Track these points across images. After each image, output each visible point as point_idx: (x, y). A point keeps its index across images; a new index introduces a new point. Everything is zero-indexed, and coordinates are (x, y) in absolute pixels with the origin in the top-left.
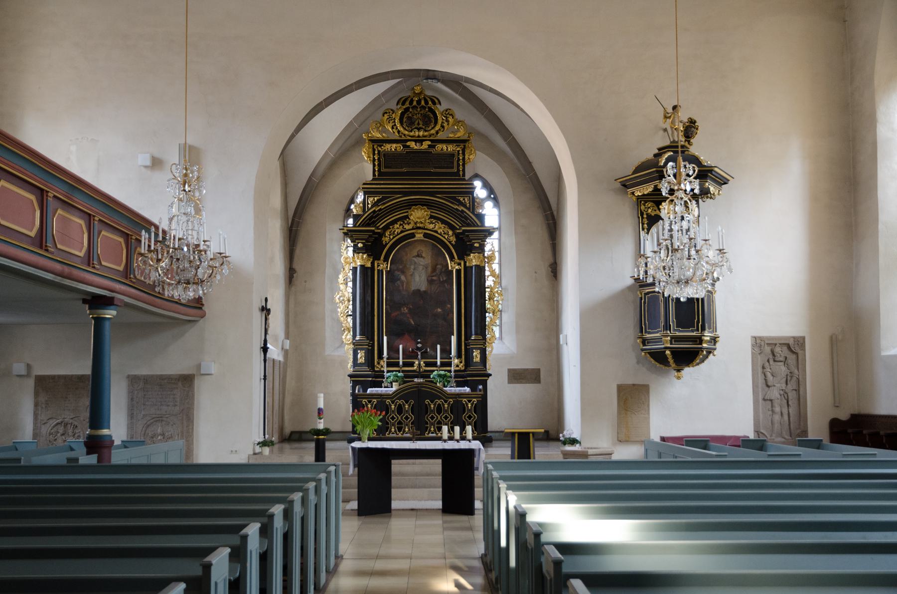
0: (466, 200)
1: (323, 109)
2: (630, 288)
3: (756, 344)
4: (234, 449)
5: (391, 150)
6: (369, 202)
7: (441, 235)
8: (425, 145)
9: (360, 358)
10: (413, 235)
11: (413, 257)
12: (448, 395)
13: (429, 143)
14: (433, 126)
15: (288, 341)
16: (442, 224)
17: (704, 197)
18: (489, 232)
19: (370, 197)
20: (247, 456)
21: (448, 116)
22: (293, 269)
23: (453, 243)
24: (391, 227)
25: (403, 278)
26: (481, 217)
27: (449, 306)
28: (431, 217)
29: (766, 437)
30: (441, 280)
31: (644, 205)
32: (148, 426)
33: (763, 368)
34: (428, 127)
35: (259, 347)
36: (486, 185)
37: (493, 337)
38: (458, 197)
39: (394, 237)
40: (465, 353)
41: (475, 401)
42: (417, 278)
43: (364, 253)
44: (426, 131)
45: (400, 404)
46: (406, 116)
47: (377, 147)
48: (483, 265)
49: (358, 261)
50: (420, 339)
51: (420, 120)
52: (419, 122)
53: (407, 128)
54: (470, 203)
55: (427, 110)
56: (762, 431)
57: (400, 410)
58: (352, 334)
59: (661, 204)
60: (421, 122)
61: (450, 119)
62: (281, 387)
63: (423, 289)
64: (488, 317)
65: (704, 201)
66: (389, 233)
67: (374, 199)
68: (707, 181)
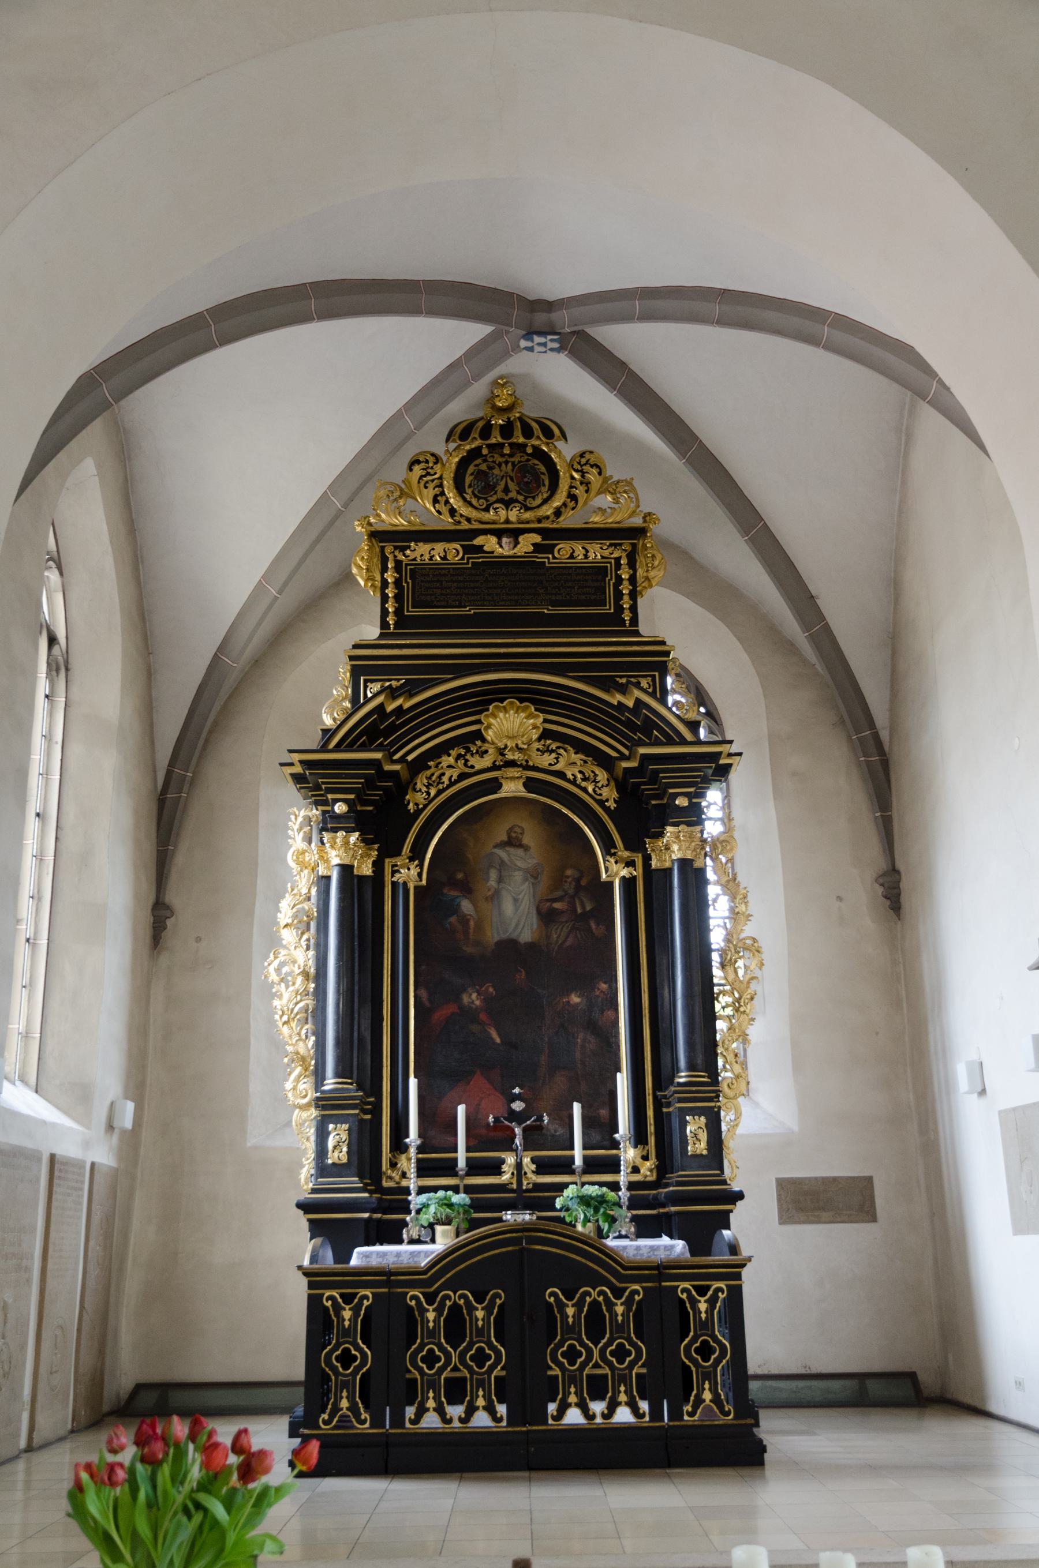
7: (574, 782)
8: (526, 543)
9: (335, 1147)
11: (495, 847)
13: (537, 538)
14: (545, 496)
19: (372, 681)
21: (586, 468)
23: (612, 805)
24: (431, 763)
25: (466, 906)
27: (604, 986)
28: (545, 735)
30: (579, 911)
34: (534, 498)
39: (439, 792)
42: (508, 907)
43: (349, 831)
44: (527, 509)
45: (455, 1307)
46: (471, 469)
50: (521, 1088)
53: (474, 501)
60: (512, 486)
61: (592, 476)
66: (425, 781)
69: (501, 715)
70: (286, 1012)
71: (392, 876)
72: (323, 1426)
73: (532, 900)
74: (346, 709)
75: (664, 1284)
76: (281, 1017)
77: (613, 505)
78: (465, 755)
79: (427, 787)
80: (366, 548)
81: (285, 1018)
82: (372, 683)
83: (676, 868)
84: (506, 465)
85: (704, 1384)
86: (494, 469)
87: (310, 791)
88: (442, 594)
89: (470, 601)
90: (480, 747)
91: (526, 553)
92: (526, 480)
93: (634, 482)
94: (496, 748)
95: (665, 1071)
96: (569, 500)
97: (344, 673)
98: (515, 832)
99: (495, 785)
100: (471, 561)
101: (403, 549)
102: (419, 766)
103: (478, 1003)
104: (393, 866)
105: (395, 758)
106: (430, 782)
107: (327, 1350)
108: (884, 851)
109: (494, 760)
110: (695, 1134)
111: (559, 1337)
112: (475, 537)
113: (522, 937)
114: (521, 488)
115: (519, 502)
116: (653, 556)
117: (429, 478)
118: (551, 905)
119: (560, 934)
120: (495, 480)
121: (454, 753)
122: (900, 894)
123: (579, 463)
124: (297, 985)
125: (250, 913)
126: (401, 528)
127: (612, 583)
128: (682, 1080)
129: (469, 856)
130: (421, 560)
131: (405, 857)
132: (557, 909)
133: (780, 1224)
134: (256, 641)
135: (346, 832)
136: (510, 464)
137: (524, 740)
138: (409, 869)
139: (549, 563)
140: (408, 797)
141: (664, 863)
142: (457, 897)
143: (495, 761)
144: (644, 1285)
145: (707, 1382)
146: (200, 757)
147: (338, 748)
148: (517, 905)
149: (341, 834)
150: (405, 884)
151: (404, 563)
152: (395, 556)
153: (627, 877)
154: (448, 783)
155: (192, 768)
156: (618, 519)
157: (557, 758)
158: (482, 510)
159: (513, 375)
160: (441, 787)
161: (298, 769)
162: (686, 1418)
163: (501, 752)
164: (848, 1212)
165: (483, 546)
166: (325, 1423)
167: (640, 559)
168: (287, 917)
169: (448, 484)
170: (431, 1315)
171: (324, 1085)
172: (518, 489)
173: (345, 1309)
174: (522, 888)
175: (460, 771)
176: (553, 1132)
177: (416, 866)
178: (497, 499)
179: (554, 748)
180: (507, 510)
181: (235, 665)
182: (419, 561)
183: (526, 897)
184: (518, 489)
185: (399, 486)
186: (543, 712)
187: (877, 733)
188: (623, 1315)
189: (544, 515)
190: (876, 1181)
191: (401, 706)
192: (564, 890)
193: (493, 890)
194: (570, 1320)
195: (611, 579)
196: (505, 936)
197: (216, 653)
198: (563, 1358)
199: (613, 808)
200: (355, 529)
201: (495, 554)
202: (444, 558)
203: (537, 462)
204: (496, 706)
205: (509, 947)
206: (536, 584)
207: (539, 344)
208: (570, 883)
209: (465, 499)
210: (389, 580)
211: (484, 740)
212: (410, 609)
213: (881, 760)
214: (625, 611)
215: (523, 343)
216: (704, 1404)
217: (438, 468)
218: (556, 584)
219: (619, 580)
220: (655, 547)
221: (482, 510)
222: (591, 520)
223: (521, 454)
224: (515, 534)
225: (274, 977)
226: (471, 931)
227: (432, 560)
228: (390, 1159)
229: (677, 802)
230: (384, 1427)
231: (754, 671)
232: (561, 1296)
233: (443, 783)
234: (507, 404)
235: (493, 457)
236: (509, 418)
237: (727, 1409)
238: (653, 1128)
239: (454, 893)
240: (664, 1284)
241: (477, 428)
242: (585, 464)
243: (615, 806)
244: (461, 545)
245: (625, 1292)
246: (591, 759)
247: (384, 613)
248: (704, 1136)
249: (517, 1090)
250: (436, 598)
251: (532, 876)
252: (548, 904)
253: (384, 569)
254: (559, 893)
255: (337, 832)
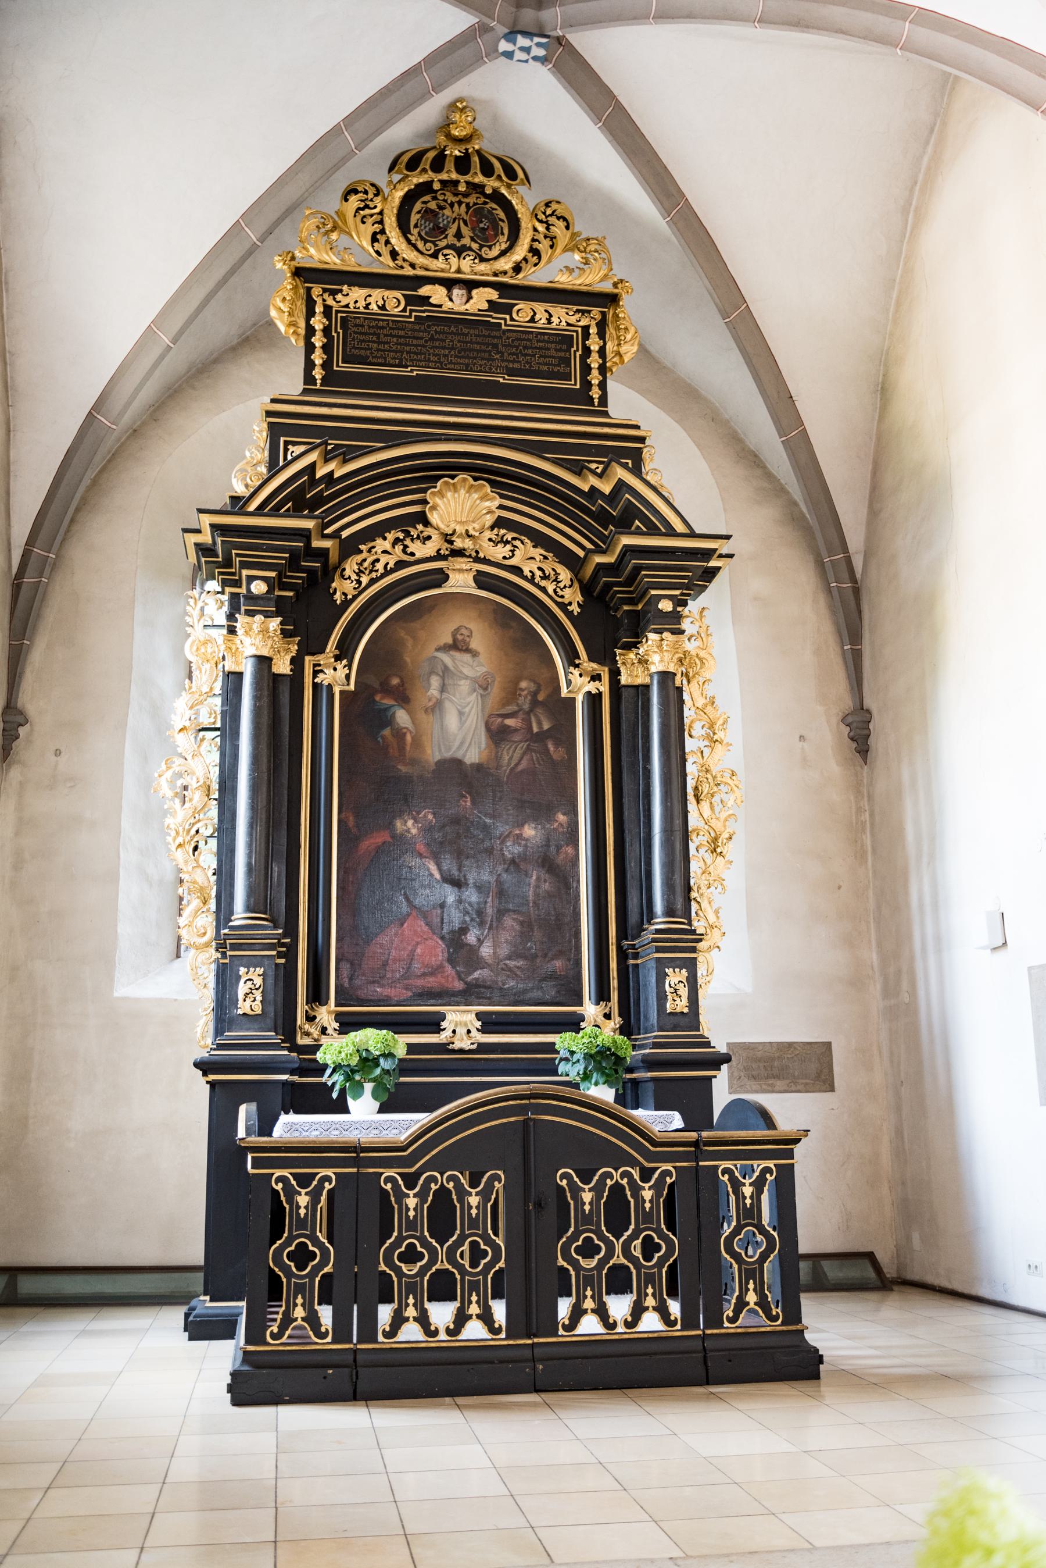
7: (531, 580)
8: (481, 298)
11: (438, 649)
13: (493, 295)
14: (504, 246)
19: (295, 444)
21: (552, 220)
23: (575, 609)
24: (362, 547)
25: (402, 717)
28: (500, 523)
30: (535, 729)
34: (490, 247)
39: (373, 581)
42: (452, 721)
44: (483, 260)
45: (443, 1191)
46: (418, 206)
53: (420, 245)
61: (559, 228)
66: (356, 567)
69: (449, 494)
70: (181, 833)
71: (315, 676)
72: (271, 1341)
73: (480, 715)
74: (261, 474)
75: (701, 1163)
76: (174, 840)
77: (582, 266)
78: (404, 539)
79: (358, 574)
80: (289, 287)
81: (180, 840)
82: (294, 445)
83: (655, 682)
85: (747, 1283)
86: (445, 209)
87: (217, 568)
88: (378, 350)
89: (412, 360)
90: (422, 532)
91: (479, 310)
92: (482, 225)
93: (606, 242)
94: (442, 533)
95: (633, 918)
96: (531, 254)
97: (260, 432)
98: (462, 634)
99: (440, 578)
100: (414, 314)
101: (333, 293)
102: (349, 547)
103: (414, 831)
104: (315, 665)
105: (327, 532)
106: (361, 568)
107: (277, 1245)
108: (852, 689)
109: (438, 548)
110: (676, 989)
111: (572, 1229)
112: (420, 287)
113: (467, 757)
114: (476, 235)
115: (474, 251)
116: (626, 329)
117: (367, 212)
118: (502, 722)
119: (512, 755)
120: (445, 222)
121: (391, 536)
122: (869, 736)
123: (544, 213)
124: (195, 802)
125: (122, 725)
126: (332, 267)
127: (578, 354)
129: (408, 660)
130: (355, 308)
131: (332, 655)
132: (509, 727)
134: (137, 405)
135: (265, 617)
136: (464, 205)
137: (477, 526)
138: (335, 669)
139: (506, 325)
140: (334, 585)
141: (635, 678)
142: (393, 706)
143: (440, 550)
144: (678, 1164)
145: (751, 1282)
146: (64, 540)
147: (260, 511)
148: (463, 719)
149: (259, 618)
150: (330, 687)
151: (334, 309)
152: (324, 300)
153: (593, 692)
154: (383, 571)
155: (55, 549)
156: (587, 282)
157: (513, 551)
158: (428, 255)
159: (474, 100)
160: (374, 575)
161: (206, 538)
162: (726, 1324)
163: (448, 538)
164: (804, 1081)
165: (429, 297)
166: (274, 1336)
167: (610, 331)
168: (184, 719)
169: (391, 222)
170: (412, 1202)
171: (231, 921)
172: (472, 235)
173: (300, 1194)
174: (468, 700)
176: (500, 984)
177: (345, 667)
179: (509, 539)
181: (114, 427)
182: (352, 309)
183: (474, 711)
184: (472, 235)
185: (332, 218)
186: (502, 496)
188: (651, 1201)
189: (501, 269)
190: (835, 1047)
191: (332, 472)
192: (518, 705)
193: (434, 700)
194: (587, 1208)
195: (578, 350)
196: (448, 755)
198: (577, 1254)
199: (576, 614)
200: (274, 265)
201: (444, 308)
202: (383, 308)
203: (495, 206)
204: (431, 493)
205: (453, 767)
206: (490, 348)
207: (522, 49)
208: (526, 697)
209: (409, 241)
210: (317, 327)
211: (427, 523)
212: (340, 364)
213: (853, 587)
214: (593, 387)
215: (504, 46)
216: (747, 1308)
217: (378, 200)
218: (514, 350)
219: (587, 351)
220: (627, 319)
221: (428, 255)
222: (556, 280)
223: (478, 195)
224: (470, 285)
225: (166, 791)
226: (408, 748)
227: (368, 309)
228: (307, 1011)
229: (660, 606)
230: (351, 1341)
231: (714, 481)
232: (576, 1179)
233: (377, 571)
234: (465, 133)
235: (445, 195)
236: (467, 150)
237: (774, 1313)
238: (616, 981)
239: (388, 702)
240: (701, 1163)
241: (427, 159)
242: (550, 215)
243: (579, 610)
244: (403, 295)
245: (654, 1173)
246: (551, 555)
247: (309, 365)
248: (684, 991)
250: (371, 353)
251: (480, 686)
252: (499, 720)
253: (310, 313)
254: (513, 708)
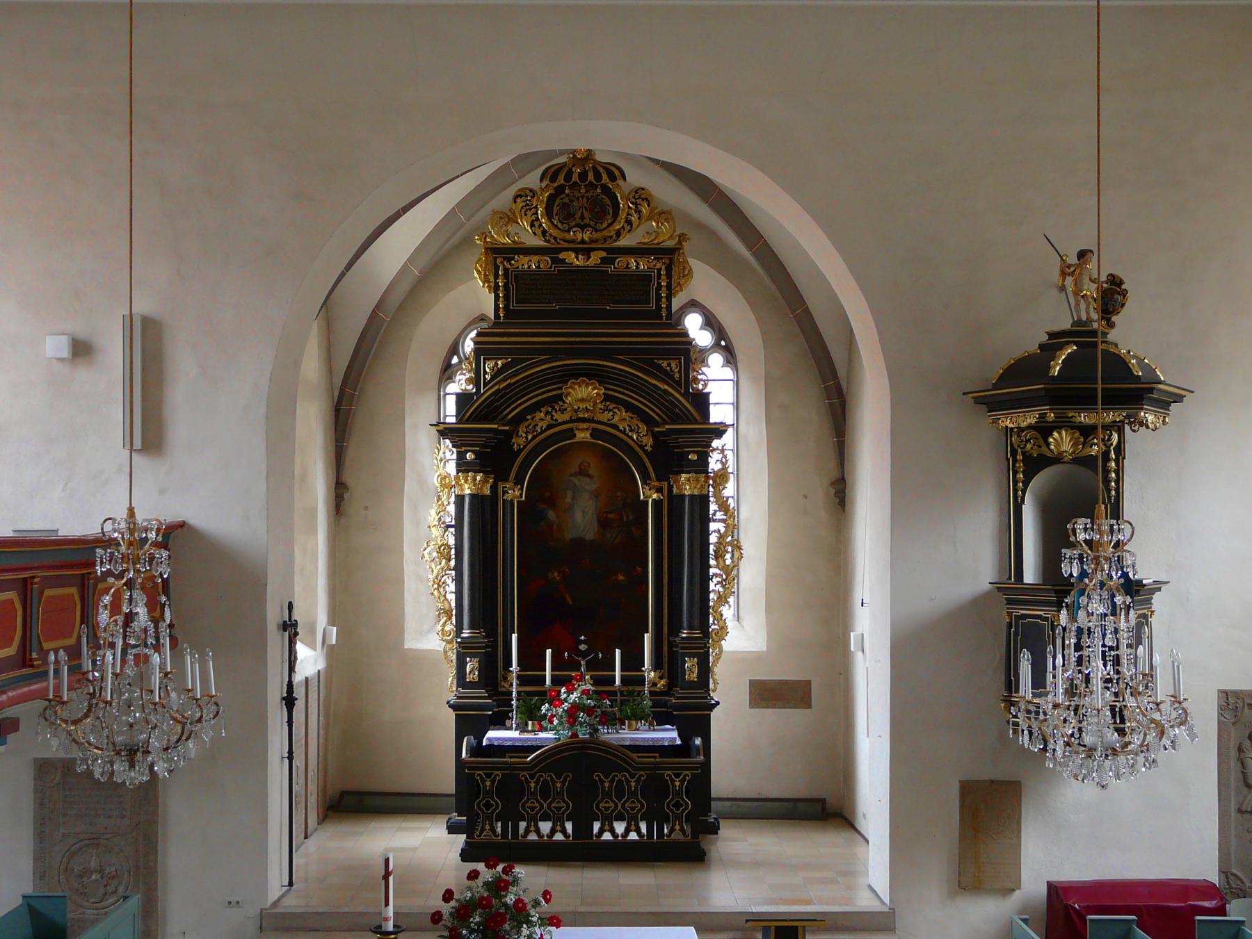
0: (673, 365)
1: (399, 218)
2: (978, 604)
3: (1228, 704)
4: (234, 899)
5: (529, 267)
6: (488, 370)
8: (595, 258)
9: (470, 672)
10: (570, 434)
11: (571, 475)
12: (637, 764)
13: (603, 254)
14: (610, 221)
15: (335, 628)
16: (626, 412)
17: (1134, 422)
18: (719, 431)
19: (489, 359)
20: (259, 911)
21: (639, 201)
22: (342, 484)
23: (648, 448)
24: (529, 417)
25: (551, 515)
26: (702, 402)
28: (607, 398)
29: (1243, 883)
30: (625, 519)
31: (1019, 436)
32: (73, 855)
33: (1240, 750)
34: (601, 223)
35: (278, 699)
36: (710, 322)
37: (722, 628)
38: (658, 359)
40: (668, 661)
41: (688, 775)
42: (579, 516)
43: (476, 472)
44: (597, 231)
45: (545, 781)
46: (558, 201)
47: (502, 263)
48: (705, 492)
49: (466, 486)
50: (585, 636)
51: (586, 208)
52: (582, 215)
53: (559, 225)
54: (680, 372)
55: (599, 190)
56: (1234, 871)
57: (545, 792)
58: (454, 622)
59: (1051, 434)
60: (586, 214)
61: (645, 209)
62: (322, 732)
63: (590, 535)
64: (713, 591)
65: (1134, 431)
66: (525, 430)
67: (496, 364)
68: (1142, 409)
79: (526, 433)
84: (582, 199)
90: (562, 406)
103: (558, 578)
123: (634, 198)
128: (684, 635)
133: (750, 708)
140: (513, 440)
143: (572, 417)
175: (548, 423)
178: (576, 224)
180: (583, 232)
185: (506, 214)
187: (839, 382)
197: (374, 309)
203: (604, 197)
205: (578, 542)
209: (553, 223)
219: (659, 286)
242: (638, 198)
244: (550, 258)
246: (636, 416)
249: (583, 638)
251: (595, 496)
252: (605, 515)
255: (468, 473)
